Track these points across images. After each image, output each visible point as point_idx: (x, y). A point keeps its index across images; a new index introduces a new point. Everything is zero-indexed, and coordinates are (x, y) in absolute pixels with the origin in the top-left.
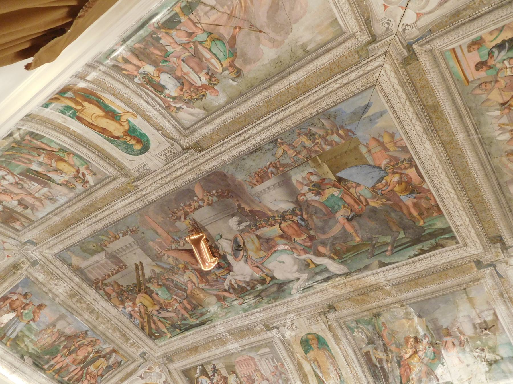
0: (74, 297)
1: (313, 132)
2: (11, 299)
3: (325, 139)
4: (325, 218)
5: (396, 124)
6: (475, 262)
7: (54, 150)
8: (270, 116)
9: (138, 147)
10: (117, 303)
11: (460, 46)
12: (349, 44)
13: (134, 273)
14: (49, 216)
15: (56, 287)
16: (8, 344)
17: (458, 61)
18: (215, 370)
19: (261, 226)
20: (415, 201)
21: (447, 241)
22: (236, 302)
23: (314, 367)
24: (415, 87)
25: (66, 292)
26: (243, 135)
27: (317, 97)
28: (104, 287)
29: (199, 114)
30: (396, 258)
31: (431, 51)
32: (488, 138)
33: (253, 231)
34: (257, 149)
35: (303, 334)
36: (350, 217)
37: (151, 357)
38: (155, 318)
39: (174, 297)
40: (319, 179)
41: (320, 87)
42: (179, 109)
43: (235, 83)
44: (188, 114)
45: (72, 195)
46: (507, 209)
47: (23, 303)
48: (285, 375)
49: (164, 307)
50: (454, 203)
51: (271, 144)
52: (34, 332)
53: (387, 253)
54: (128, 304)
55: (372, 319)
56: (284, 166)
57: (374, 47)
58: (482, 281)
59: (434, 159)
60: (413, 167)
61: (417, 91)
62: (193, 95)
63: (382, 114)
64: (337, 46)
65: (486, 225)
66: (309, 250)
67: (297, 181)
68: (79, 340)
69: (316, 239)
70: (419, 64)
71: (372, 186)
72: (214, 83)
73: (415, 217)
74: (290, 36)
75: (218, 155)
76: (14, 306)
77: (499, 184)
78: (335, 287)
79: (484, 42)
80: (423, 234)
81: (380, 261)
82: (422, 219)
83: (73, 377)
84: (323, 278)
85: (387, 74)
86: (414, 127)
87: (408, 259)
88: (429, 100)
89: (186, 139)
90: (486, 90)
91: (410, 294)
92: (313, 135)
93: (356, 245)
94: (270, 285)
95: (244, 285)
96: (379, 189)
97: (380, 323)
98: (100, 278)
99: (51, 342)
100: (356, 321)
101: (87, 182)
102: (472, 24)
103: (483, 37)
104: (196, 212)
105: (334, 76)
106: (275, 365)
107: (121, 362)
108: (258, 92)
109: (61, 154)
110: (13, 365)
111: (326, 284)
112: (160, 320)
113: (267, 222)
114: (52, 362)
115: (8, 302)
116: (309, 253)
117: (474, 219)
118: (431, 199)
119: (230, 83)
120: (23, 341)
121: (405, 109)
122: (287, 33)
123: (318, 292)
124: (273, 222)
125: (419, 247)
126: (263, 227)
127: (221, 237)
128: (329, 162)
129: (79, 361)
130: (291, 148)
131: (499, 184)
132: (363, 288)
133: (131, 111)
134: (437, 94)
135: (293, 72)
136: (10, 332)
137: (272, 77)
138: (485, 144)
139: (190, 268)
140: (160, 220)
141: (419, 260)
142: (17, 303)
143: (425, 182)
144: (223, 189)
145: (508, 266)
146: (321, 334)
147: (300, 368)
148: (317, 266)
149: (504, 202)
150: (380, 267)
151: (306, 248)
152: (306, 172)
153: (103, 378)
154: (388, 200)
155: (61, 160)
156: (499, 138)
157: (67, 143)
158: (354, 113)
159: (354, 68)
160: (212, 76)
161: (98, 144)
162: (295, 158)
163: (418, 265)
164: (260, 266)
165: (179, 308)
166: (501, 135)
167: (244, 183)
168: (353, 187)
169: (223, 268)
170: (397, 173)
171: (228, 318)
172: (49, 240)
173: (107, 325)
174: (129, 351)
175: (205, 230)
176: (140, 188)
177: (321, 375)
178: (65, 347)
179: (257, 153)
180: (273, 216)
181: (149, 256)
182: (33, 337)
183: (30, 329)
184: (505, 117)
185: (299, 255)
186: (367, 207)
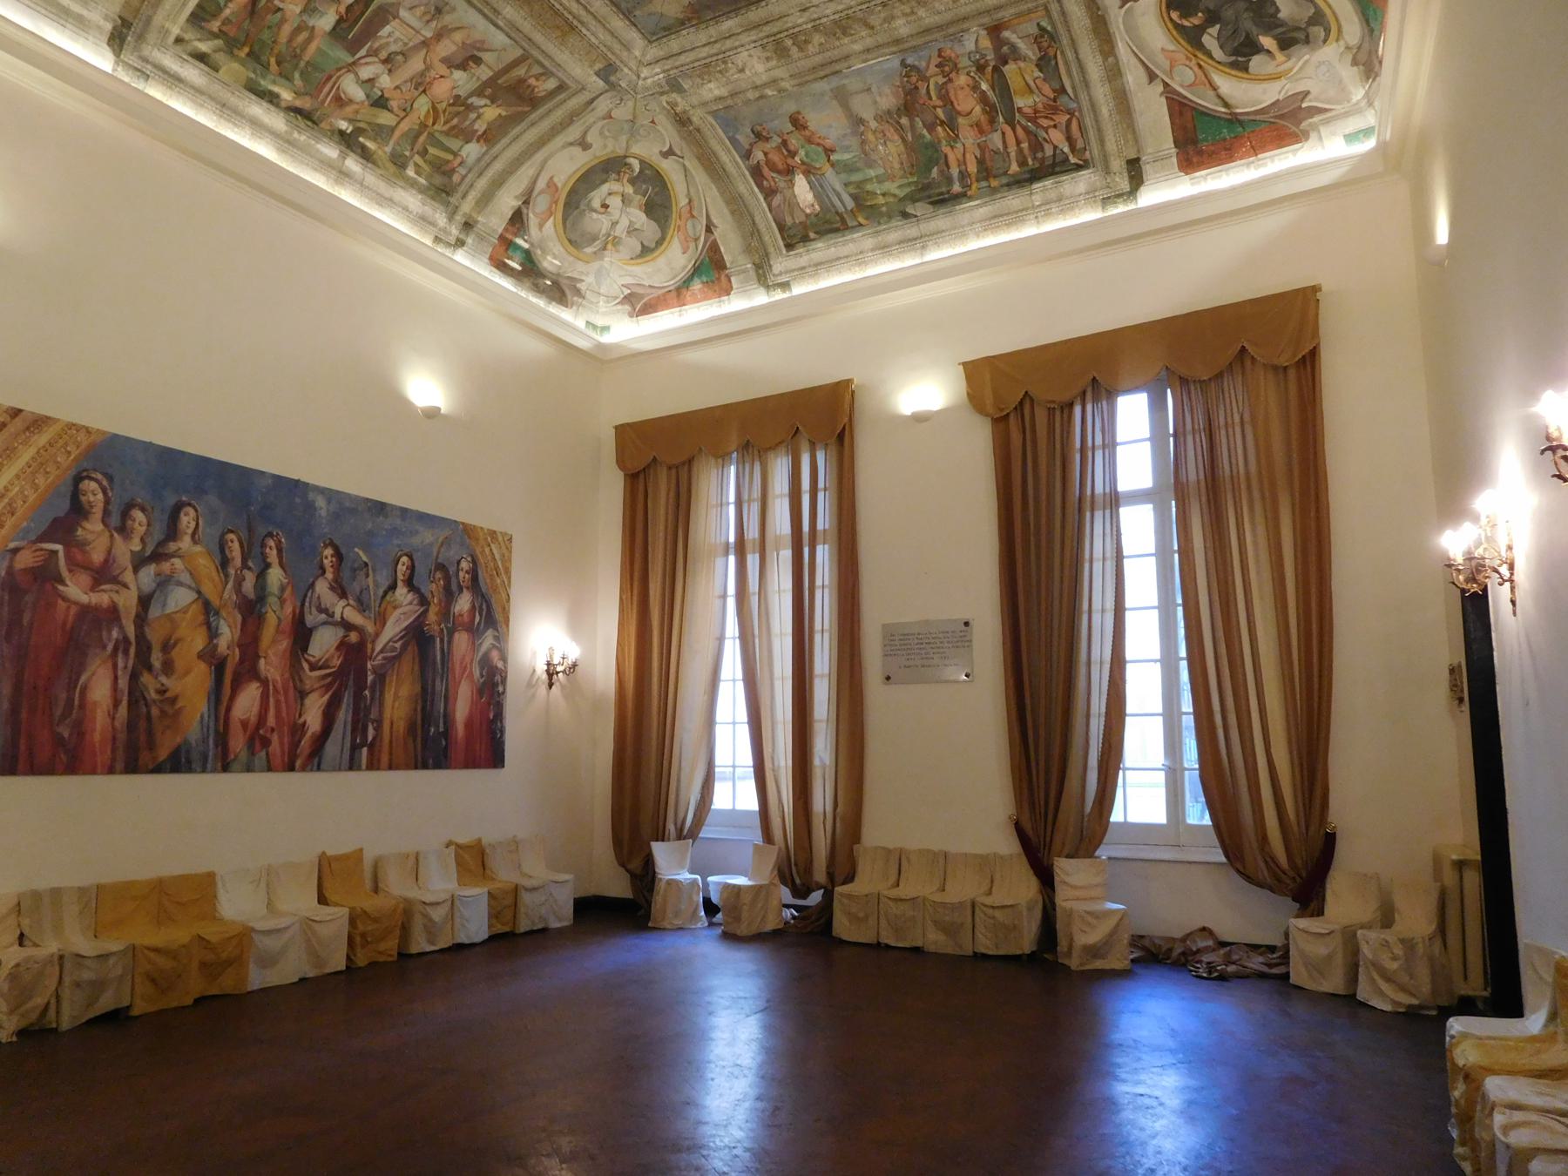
14: (501, 23)
16: (861, 220)
25: (768, 59)
47: (778, 148)
68: (924, 91)
76: (780, 166)
83: (1020, 151)
99: (902, 148)
107: (1042, 29)
114: (955, 172)
115: (766, 171)
136: (838, 204)
153: (1070, 91)
172: (593, 40)
173: (897, 12)
178: (931, 128)
182: (872, 173)
183: (849, 168)
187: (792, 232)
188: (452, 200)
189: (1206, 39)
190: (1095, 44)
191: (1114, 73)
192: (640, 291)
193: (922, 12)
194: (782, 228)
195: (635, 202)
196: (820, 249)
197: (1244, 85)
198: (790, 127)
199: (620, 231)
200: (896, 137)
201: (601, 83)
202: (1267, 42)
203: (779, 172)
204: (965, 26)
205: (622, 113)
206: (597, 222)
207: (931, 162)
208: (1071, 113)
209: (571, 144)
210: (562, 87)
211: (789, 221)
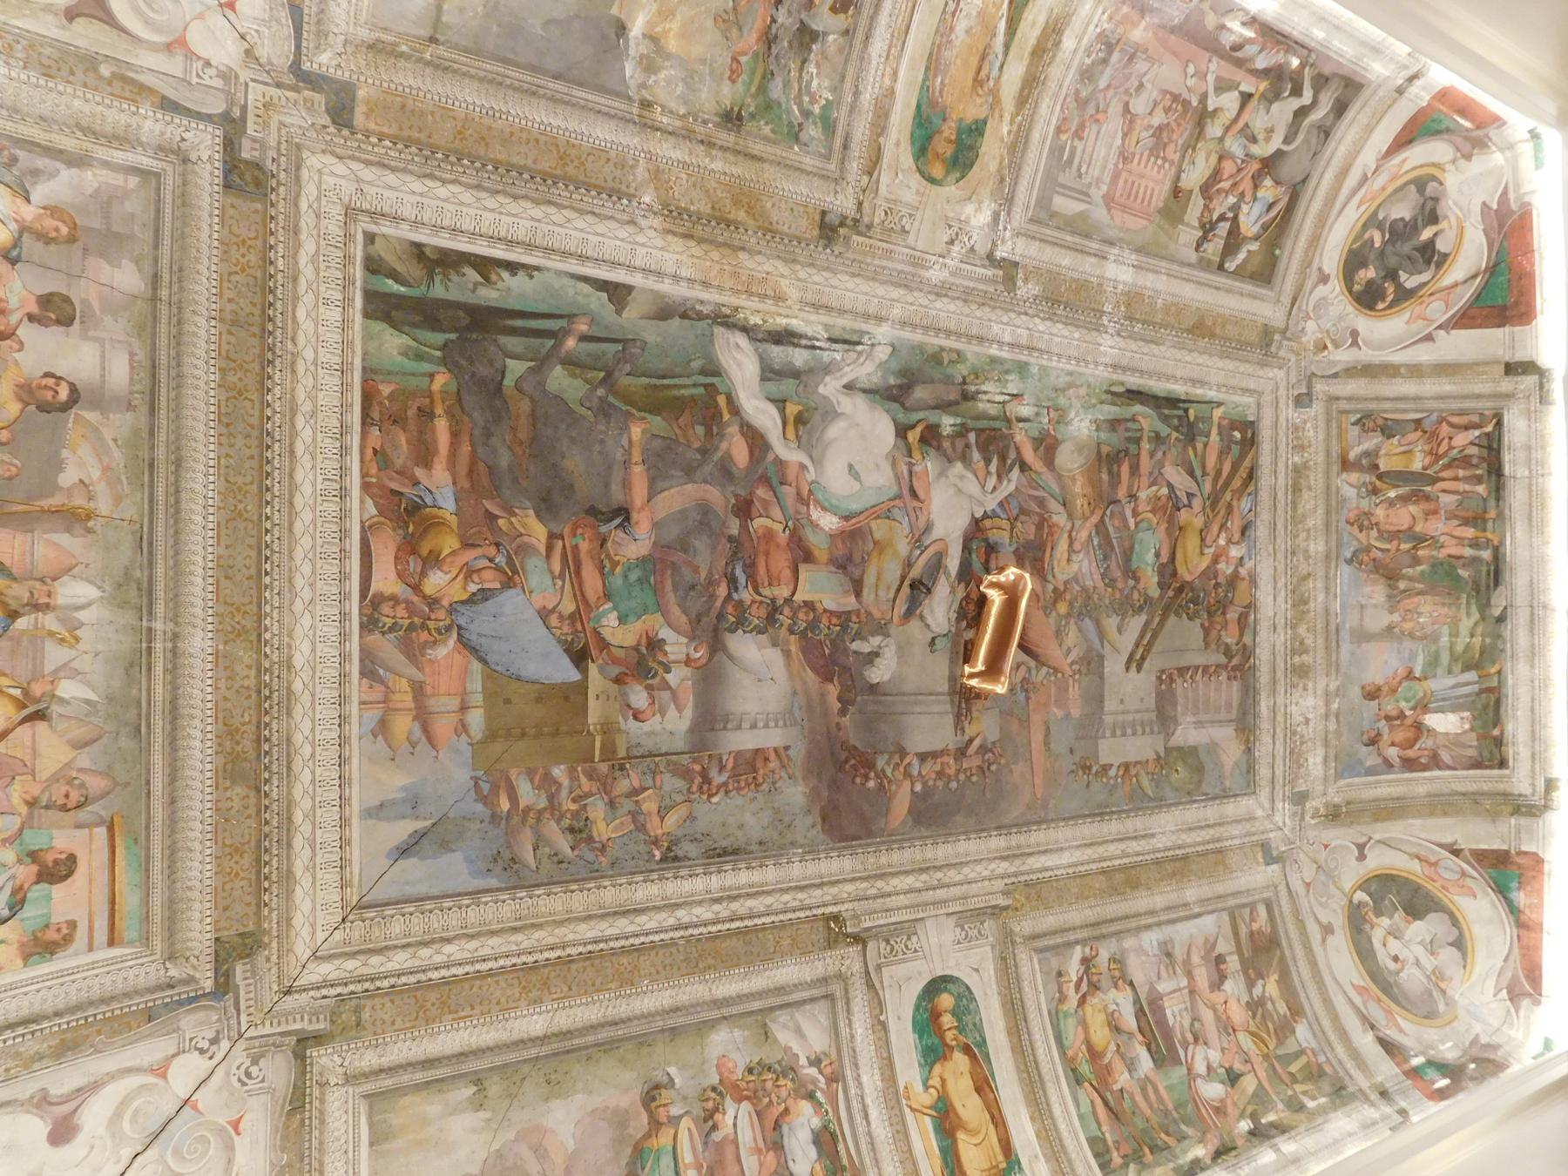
0: (1302, 665)
1: (570, 837)
2: (1401, 753)
3: (553, 806)
4: (678, 557)
5: (355, 761)
6: (350, 126)
7: (1090, 1089)
8: (643, 939)
9: (946, 1001)
10: (1243, 586)
11: (91, 949)
12: (369, 1059)
13: (1159, 645)
14: (1197, 910)
15: (1310, 716)
17: (112, 902)
18: (1207, 229)
19: (834, 620)
20: (419, 472)
21: (400, 268)
22: (1025, 411)
23: (998, 64)
24: (258, 860)
25: (1305, 689)
26: (725, 914)
27: (513, 938)
28: (1234, 647)
29: (785, 1026)
30: (571, 292)
31: (171, 957)
32: (124, 605)
33: (858, 616)
34: (719, 856)
35: (951, 190)
36: (617, 521)
37: (1293, 380)
38: (1207, 487)
39: (1132, 522)
40: (628, 689)
41: (491, 964)
42: (816, 1062)
43: (672, 1070)
44: (804, 1036)
45: (1129, 943)
46: (164, 293)
47: (1392, 728)
48: (1077, 92)
49: (1172, 506)
50: (314, 400)
51: (680, 854)
52: (1433, 648)
53: (583, 328)
54: (1225, 568)
55: (753, 116)
56: (686, 774)
57: (310, 1021)
58: (364, 34)
59: (307, 594)
60: (374, 596)
61: (259, 842)
62: (769, 1085)
63: (378, 811)
64: (400, 1066)
65: (253, 258)
66: (772, 471)
67: (680, 711)
68: (1379, 554)
69: (736, 496)
70: (222, 924)
71: (511, 592)
72: (713, 1095)
73: (450, 414)
74: (496, 1146)
75: (806, 886)
76: (1410, 734)
77: (153, 410)
78: (779, 298)
79: (22, 945)
80: (453, 336)
81: (619, 312)
82: (430, 395)
83: (1466, 479)
84: (791, 349)
85: (313, 926)
86: (313, 730)
87: (537, 269)
88: (236, 804)
89: (843, 969)
90: (70, 781)
91: (603, 133)
92: (572, 830)
93: (650, 412)
94: (921, 415)
95: (976, 456)
96: (498, 568)
97: (740, 86)
98: (1224, 676)
99: (1428, 598)
100: (797, 139)
101: (1085, 961)
102: (37, 1008)
103: (19, 962)
104: (938, 746)
105: (446, 982)
106: (1076, 142)
108: (636, 1022)
109: (1085, 1069)
110: (1532, 621)
111: (794, 322)
112: (1204, 474)
113: (813, 625)
114: (1468, 552)
115: (1411, 753)
116: (780, 464)
117: (279, 305)
118: (375, 452)
119: (684, 1075)
120: (1468, 646)
121: (313, 799)
122: (499, 1155)
123: (828, 308)
124: (801, 615)
125: (488, 296)
126: (831, 613)
127: (933, 639)
128: (579, 727)
129: (1424, 506)
130: (641, 819)
131: (153, 410)
132: (711, 242)
133: (907, 1111)
134: (209, 813)
135: (534, 1041)
137: (586, 1048)
138: (141, 592)
139: (1050, 587)
140: (1018, 769)
141: (510, 243)
142: (1400, 736)
143: (363, 527)
144: (850, 785)
145: (253, 38)
146: (907, 161)
147: (1032, 84)
148: (780, 403)
149: (163, 329)
150: (629, 289)
151: (775, 481)
152: (646, 727)
154: (492, 518)
155: (1094, 1054)
156: (91, 592)
157: (1059, 1094)
158: (445, 846)
159: (386, 983)
160: (710, 1115)
161: (1009, 1054)
162: (650, 783)
163: (522, 230)
164: (906, 492)
165: (1145, 481)
166: (83, 600)
167: (799, 774)
168: (561, 617)
169: (986, 540)
170: (424, 597)
171: (1070, 374)
172: (1237, 842)
174: (1321, 437)
175: (954, 679)
176: (999, 885)
177: (1002, 25)
178: (1416, 561)
179: (724, 843)
180: (791, 632)
181: (1102, 677)
182: (1445, 639)
183: (1433, 662)
184: (49, 668)
185: (803, 467)
186: (556, 530)
187: (1486, 754)
188: (1351, 1089)
189: (1408, 285)
190: (1384, 380)
191: (1416, 371)
192: (1508, 975)
193: (1310, 523)
194: (1477, 765)
195: (1402, 925)
196: (1516, 727)
197: (1460, 259)
198: (1374, 703)
199: (1428, 962)
200: (1416, 600)
201: (1275, 867)
202: (1426, 234)
203: (1416, 740)
204: (1334, 489)
205: (1309, 872)
206: (1411, 979)
207: (1451, 574)
208: (1441, 420)
209: (1324, 940)
210: (1269, 905)
211: (1472, 753)
